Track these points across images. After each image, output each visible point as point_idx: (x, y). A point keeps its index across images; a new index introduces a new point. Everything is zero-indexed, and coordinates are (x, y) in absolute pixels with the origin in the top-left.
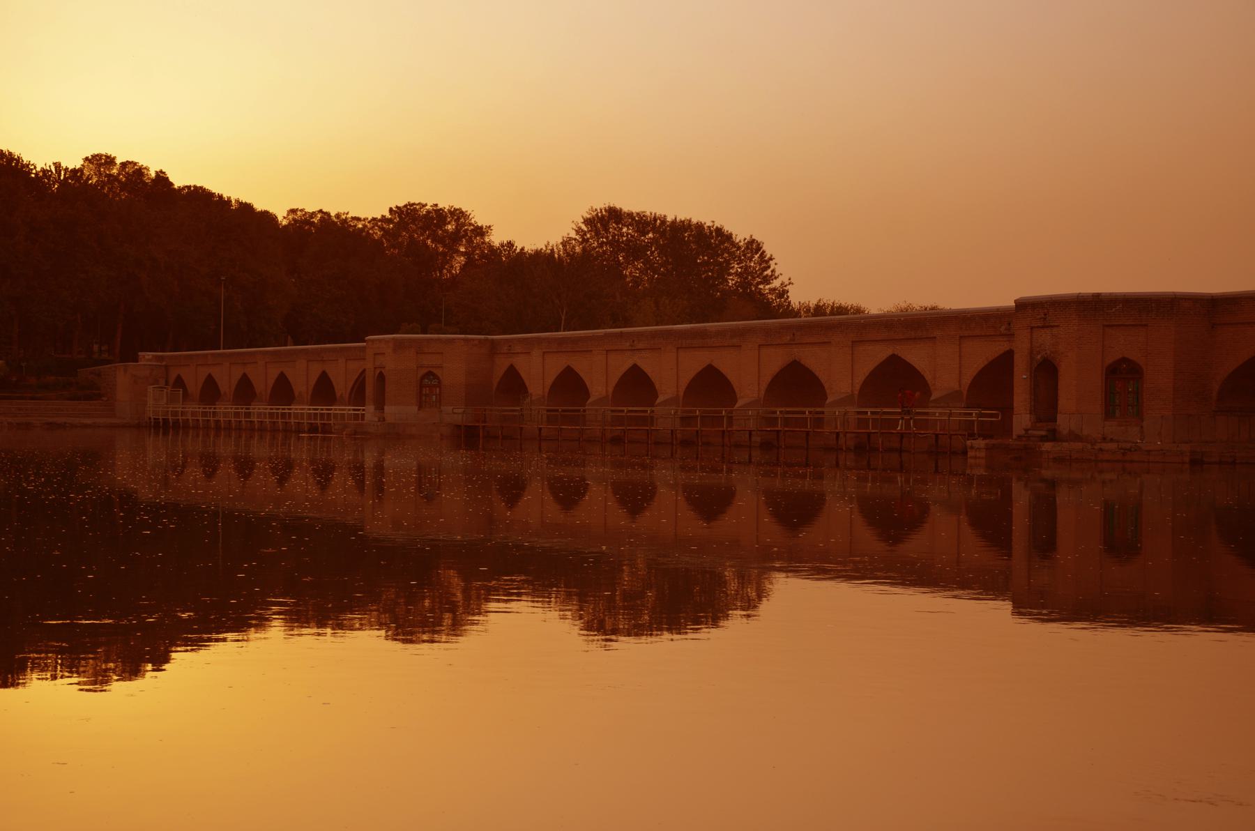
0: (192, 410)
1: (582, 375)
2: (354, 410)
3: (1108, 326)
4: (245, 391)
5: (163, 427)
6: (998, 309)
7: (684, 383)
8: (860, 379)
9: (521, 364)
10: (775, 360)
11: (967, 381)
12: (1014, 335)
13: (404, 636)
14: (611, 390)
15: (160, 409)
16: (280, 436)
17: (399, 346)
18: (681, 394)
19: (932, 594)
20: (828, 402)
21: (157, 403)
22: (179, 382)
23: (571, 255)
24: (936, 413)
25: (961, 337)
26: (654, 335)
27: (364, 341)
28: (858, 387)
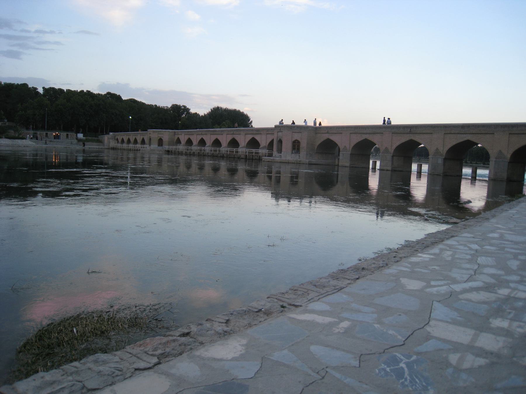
0: (119, 145)
1: (192, 140)
2: (187, 148)
3: (293, 132)
4: (129, 141)
5: (113, 149)
6: (260, 128)
7: (212, 142)
8: (246, 142)
9: (180, 137)
10: (249, 137)
11: (267, 144)
12: (274, 134)
13: (51, 154)
14: (197, 143)
15: (223, 150)
16: (116, 150)
17: (154, 132)
18: (245, 145)
19: (369, 213)
20: (260, 147)
21: (113, 144)
22: (117, 139)
23: (65, 131)
24: (260, 151)
25: (267, 134)
26: (206, 131)
27: (147, 131)
28: (246, 144)
